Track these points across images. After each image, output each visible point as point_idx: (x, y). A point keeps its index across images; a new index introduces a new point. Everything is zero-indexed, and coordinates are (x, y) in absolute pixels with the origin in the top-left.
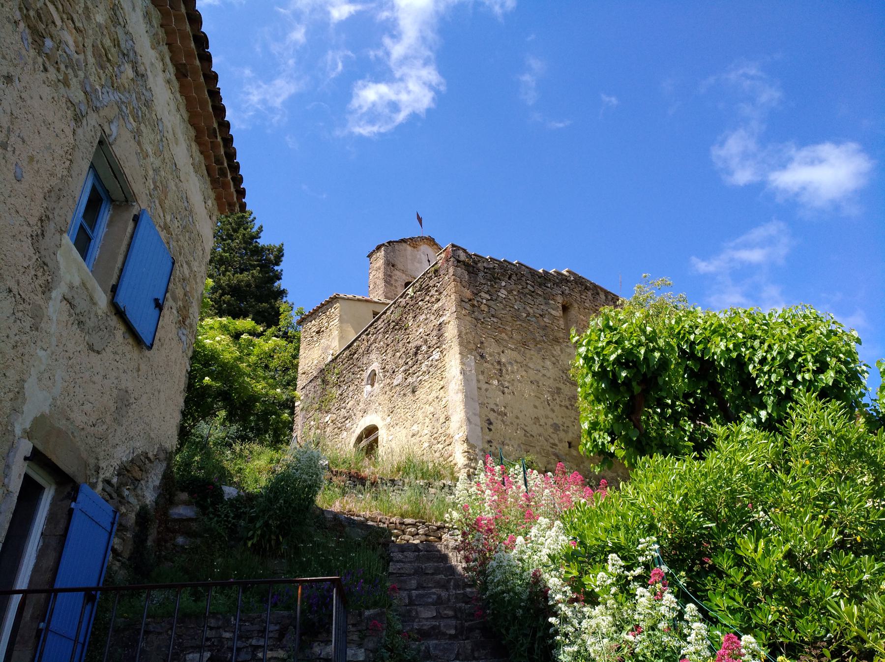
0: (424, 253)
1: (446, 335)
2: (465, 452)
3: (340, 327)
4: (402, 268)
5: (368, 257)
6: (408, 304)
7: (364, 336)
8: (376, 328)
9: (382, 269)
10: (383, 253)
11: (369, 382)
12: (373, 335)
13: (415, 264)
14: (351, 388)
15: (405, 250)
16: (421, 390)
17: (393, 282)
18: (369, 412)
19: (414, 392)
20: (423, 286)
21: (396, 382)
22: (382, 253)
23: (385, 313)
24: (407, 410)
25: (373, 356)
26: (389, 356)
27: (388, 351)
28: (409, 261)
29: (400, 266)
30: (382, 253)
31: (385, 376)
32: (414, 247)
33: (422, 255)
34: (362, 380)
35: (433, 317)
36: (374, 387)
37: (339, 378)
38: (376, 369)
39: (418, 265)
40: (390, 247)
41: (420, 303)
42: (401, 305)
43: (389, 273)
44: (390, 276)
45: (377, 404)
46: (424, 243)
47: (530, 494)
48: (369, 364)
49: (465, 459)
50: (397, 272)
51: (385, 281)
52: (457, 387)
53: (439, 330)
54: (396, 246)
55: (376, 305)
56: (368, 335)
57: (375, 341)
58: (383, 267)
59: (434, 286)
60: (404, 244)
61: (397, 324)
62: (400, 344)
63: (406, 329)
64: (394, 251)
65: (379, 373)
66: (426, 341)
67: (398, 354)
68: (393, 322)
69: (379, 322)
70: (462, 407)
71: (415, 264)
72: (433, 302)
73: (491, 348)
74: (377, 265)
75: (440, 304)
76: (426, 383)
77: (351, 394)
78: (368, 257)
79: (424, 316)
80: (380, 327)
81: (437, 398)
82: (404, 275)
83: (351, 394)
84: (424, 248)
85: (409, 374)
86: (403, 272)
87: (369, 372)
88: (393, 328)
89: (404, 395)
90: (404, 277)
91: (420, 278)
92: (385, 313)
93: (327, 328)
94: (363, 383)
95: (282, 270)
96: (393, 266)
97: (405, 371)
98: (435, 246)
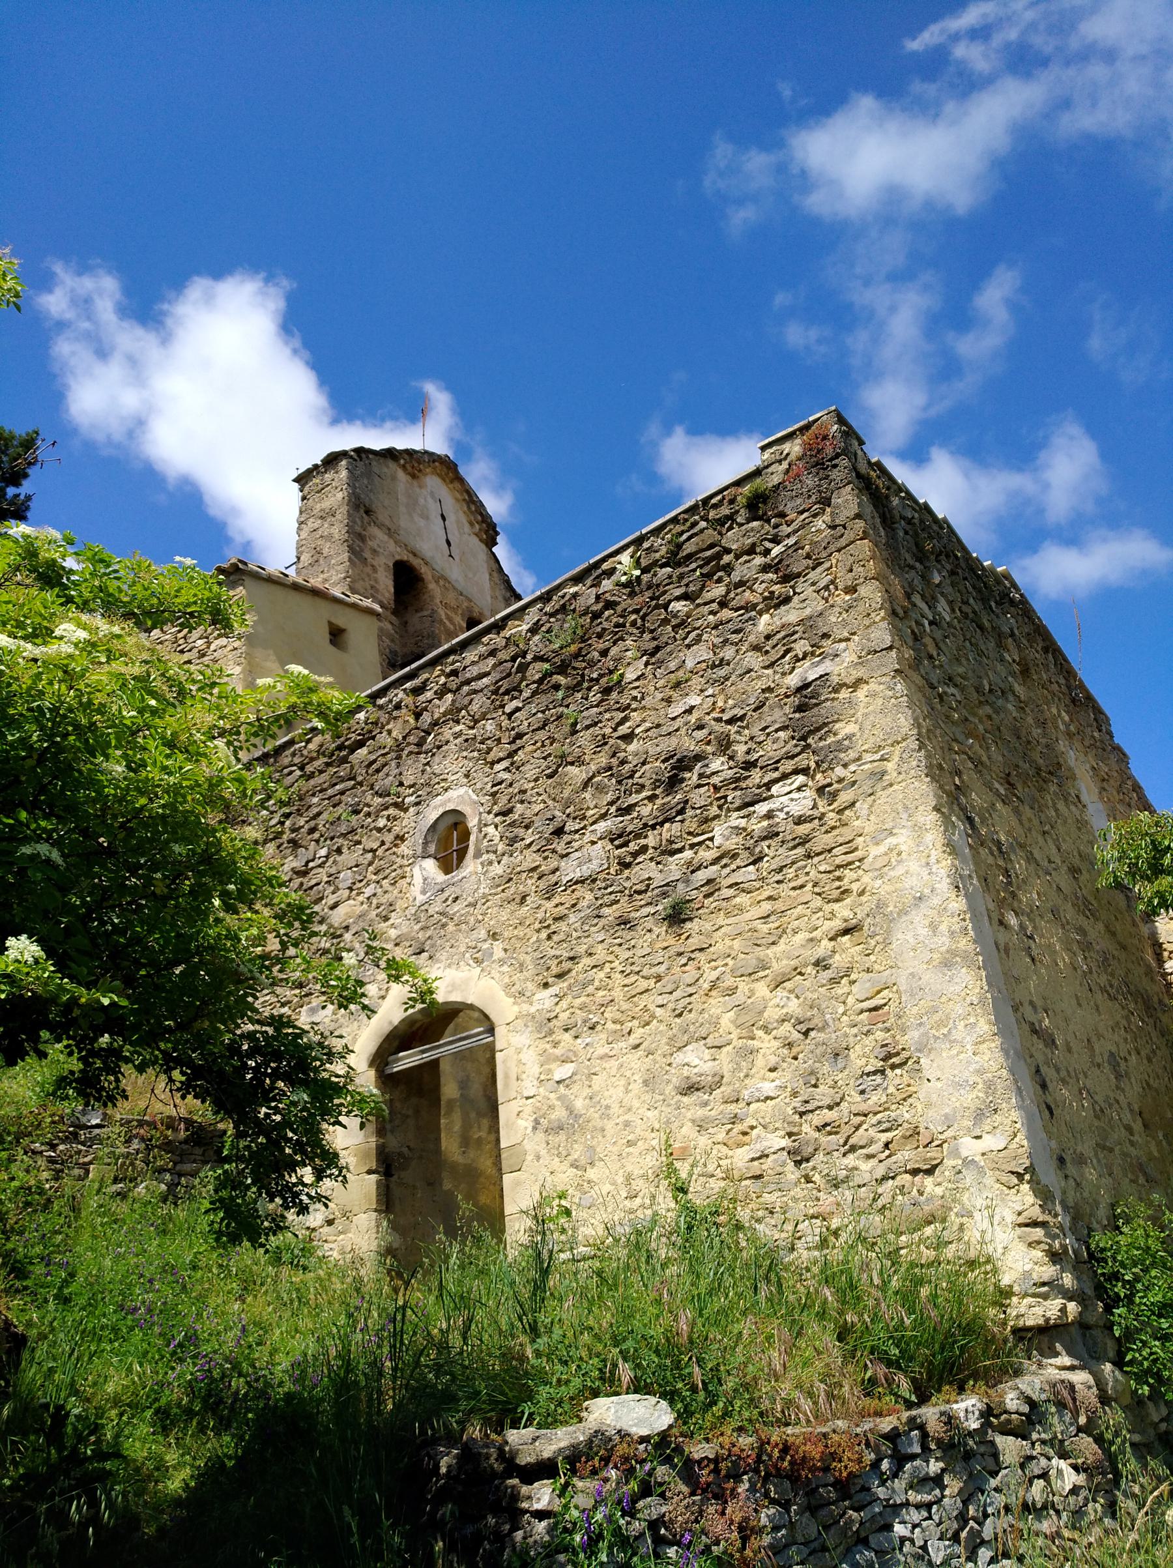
0: (432, 494)
1: (844, 729)
2: (1034, 1224)
3: (248, 655)
4: (387, 523)
5: (296, 480)
6: (609, 605)
7: (399, 695)
8: (455, 673)
9: (342, 514)
10: (344, 474)
11: (432, 849)
12: (440, 695)
13: (416, 518)
14: (347, 858)
15: (394, 478)
16: (721, 919)
17: (367, 554)
18: (442, 956)
19: (677, 917)
20: (689, 548)
21: (571, 870)
22: (342, 473)
23: (498, 627)
24: (643, 984)
25: (450, 764)
26: (530, 771)
27: (520, 756)
28: (402, 509)
29: (382, 516)
30: (342, 473)
31: (513, 841)
32: (414, 476)
33: (430, 500)
34: (401, 838)
35: (754, 660)
36: (457, 875)
37: (287, 816)
38: (467, 810)
39: (422, 523)
40: (360, 464)
41: (676, 606)
42: (580, 604)
43: (358, 529)
44: (362, 538)
45: (483, 934)
46: (435, 472)
47: (683, 1168)
48: (430, 787)
49: (1038, 1254)
50: (374, 530)
51: (351, 549)
52: (943, 942)
53: (801, 708)
54: (376, 466)
55: (337, 607)
56: (417, 691)
57: (453, 715)
58: (344, 509)
59: (751, 551)
60: (392, 465)
61: (562, 669)
62: (585, 738)
63: (607, 691)
64: (369, 474)
65: (482, 825)
66: (724, 745)
67: (576, 774)
68: (538, 658)
69: (470, 655)
70: (984, 1026)
71: (416, 518)
72: (748, 607)
73: (976, 799)
74: (326, 504)
75: (790, 615)
76: (742, 899)
77: (346, 877)
78: (296, 480)
79: (702, 653)
80: (474, 671)
81: (821, 964)
82: (392, 542)
83: (346, 877)
84: (433, 482)
85: (644, 849)
86: (390, 533)
87: (432, 814)
88: (540, 682)
89: (624, 922)
90: (391, 546)
91: (674, 520)
92: (498, 627)
93: (202, 655)
94: (404, 849)
95: (28, 498)
96: (368, 512)
97: (618, 838)
98: (457, 485)
